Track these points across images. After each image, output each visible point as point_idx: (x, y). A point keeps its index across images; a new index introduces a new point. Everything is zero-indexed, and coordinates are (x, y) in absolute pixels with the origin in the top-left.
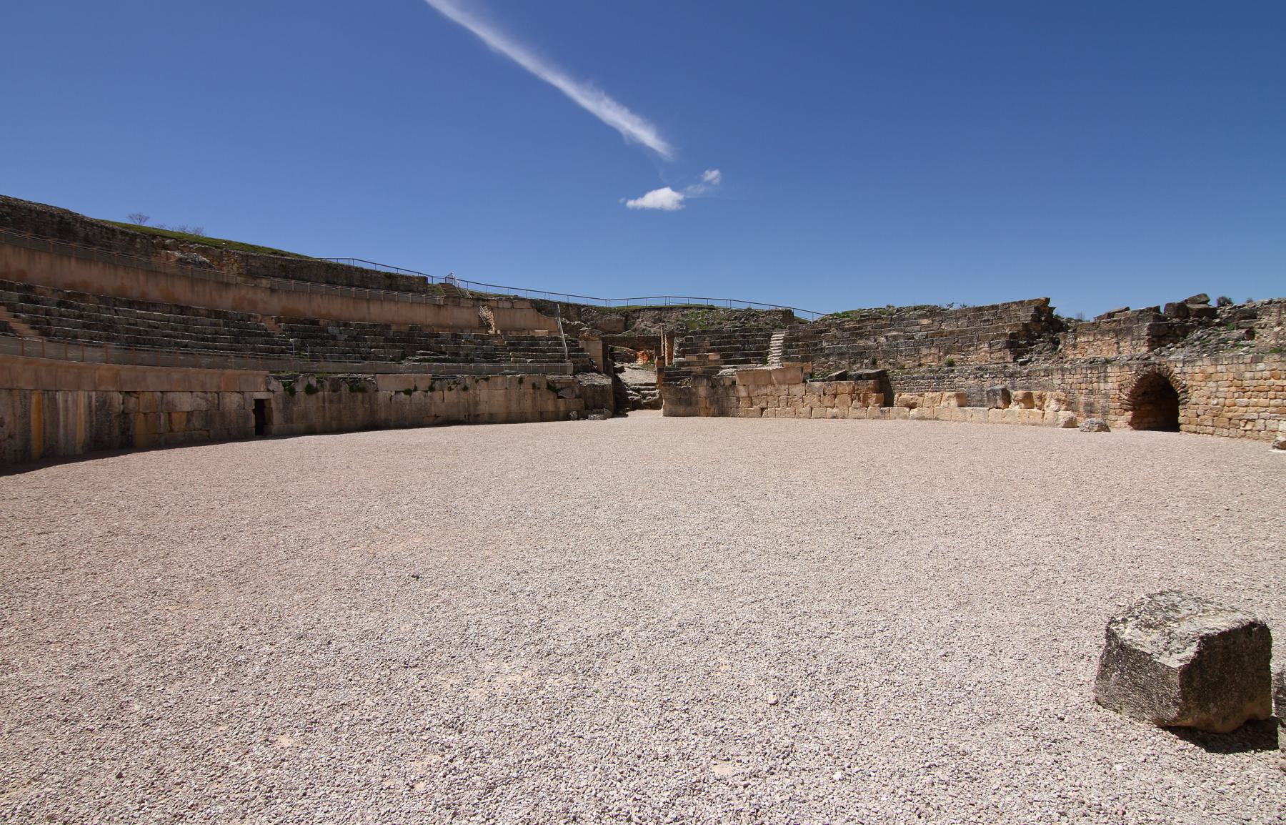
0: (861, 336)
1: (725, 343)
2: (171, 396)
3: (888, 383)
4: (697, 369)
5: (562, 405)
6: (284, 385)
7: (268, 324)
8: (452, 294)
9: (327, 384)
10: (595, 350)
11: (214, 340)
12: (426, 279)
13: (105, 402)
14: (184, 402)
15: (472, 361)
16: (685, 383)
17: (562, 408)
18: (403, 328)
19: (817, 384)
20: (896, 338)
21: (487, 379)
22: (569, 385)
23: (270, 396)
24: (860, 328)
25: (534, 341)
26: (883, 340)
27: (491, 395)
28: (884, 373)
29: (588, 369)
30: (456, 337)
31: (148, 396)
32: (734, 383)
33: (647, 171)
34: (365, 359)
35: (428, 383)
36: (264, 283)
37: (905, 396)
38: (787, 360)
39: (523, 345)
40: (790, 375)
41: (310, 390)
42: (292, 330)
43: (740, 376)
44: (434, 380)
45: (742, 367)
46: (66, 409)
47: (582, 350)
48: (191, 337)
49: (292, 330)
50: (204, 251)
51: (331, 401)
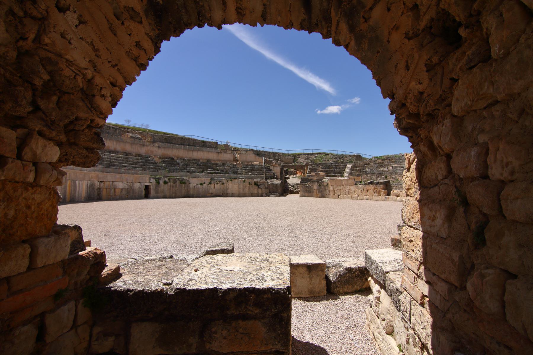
0: (382, 166)
1: (327, 168)
2: (115, 183)
3: (390, 186)
4: (315, 179)
5: (260, 191)
6: (156, 181)
7: (156, 159)
8: (226, 148)
9: (172, 180)
10: (277, 170)
11: (136, 165)
12: (217, 143)
13: (93, 184)
14: (120, 185)
15: (228, 173)
16: (309, 184)
17: (260, 192)
18: (204, 161)
19: (361, 186)
20: (396, 167)
21: (231, 180)
22: (263, 184)
23: (150, 184)
24: (383, 163)
25: (253, 166)
26: (391, 168)
27: (233, 186)
28: (389, 182)
29: (272, 178)
30: (224, 164)
31: (107, 183)
32: (328, 184)
33: (325, 99)
34: (188, 172)
35: (209, 181)
36: (156, 145)
37: (395, 192)
38: (351, 175)
39: (249, 168)
40: (350, 181)
41: (165, 183)
42: (164, 161)
43: (330, 182)
44: (211, 180)
45: (332, 178)
46: (79, 186)
47: (271, 170)
48: (128, 164)
49: (164, 161)
50: (140, 134)
51: (173, 187)
